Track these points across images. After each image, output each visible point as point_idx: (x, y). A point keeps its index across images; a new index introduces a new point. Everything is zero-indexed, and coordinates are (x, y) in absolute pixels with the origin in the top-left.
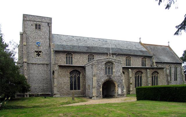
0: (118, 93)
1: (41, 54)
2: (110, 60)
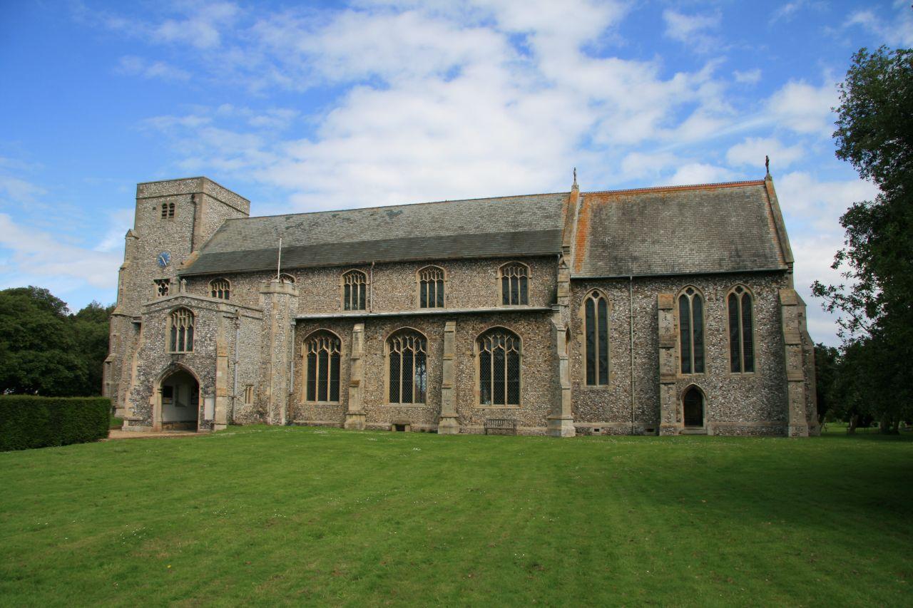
0: (203, 415)
2: (186, 301)
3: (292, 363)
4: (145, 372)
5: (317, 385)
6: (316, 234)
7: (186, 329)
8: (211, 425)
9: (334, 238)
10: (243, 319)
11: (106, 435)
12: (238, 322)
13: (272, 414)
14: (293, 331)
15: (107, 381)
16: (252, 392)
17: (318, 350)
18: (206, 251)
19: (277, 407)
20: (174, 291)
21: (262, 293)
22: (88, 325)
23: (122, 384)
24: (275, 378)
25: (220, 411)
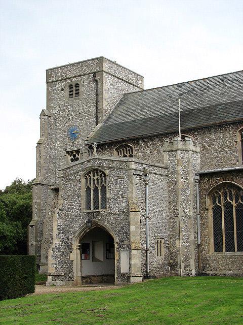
0: (119, 268)
1: (79, 157)
3: (198, 216)
4: (64, 231)
5: (224, 236)
6: (208, 97)
7: (99, 188)
8: (127, 277)
9: (226, 99)
10: (151, 176)
11: (32, 291)
12: (147, 179)
13: (182, 267)
14: (197, 186)
15: (32, 242)
16: (163, 245)
17: (223, 203)
18: (109, 123)
19: (187, 259)
20: (84, 157)
21: (166, 152)
22: (12, 197)
23: (44, 244)
24: (183, 230)
25: (135, 264)
